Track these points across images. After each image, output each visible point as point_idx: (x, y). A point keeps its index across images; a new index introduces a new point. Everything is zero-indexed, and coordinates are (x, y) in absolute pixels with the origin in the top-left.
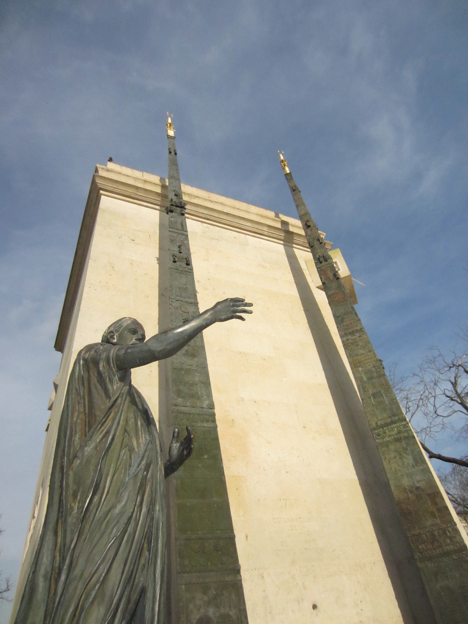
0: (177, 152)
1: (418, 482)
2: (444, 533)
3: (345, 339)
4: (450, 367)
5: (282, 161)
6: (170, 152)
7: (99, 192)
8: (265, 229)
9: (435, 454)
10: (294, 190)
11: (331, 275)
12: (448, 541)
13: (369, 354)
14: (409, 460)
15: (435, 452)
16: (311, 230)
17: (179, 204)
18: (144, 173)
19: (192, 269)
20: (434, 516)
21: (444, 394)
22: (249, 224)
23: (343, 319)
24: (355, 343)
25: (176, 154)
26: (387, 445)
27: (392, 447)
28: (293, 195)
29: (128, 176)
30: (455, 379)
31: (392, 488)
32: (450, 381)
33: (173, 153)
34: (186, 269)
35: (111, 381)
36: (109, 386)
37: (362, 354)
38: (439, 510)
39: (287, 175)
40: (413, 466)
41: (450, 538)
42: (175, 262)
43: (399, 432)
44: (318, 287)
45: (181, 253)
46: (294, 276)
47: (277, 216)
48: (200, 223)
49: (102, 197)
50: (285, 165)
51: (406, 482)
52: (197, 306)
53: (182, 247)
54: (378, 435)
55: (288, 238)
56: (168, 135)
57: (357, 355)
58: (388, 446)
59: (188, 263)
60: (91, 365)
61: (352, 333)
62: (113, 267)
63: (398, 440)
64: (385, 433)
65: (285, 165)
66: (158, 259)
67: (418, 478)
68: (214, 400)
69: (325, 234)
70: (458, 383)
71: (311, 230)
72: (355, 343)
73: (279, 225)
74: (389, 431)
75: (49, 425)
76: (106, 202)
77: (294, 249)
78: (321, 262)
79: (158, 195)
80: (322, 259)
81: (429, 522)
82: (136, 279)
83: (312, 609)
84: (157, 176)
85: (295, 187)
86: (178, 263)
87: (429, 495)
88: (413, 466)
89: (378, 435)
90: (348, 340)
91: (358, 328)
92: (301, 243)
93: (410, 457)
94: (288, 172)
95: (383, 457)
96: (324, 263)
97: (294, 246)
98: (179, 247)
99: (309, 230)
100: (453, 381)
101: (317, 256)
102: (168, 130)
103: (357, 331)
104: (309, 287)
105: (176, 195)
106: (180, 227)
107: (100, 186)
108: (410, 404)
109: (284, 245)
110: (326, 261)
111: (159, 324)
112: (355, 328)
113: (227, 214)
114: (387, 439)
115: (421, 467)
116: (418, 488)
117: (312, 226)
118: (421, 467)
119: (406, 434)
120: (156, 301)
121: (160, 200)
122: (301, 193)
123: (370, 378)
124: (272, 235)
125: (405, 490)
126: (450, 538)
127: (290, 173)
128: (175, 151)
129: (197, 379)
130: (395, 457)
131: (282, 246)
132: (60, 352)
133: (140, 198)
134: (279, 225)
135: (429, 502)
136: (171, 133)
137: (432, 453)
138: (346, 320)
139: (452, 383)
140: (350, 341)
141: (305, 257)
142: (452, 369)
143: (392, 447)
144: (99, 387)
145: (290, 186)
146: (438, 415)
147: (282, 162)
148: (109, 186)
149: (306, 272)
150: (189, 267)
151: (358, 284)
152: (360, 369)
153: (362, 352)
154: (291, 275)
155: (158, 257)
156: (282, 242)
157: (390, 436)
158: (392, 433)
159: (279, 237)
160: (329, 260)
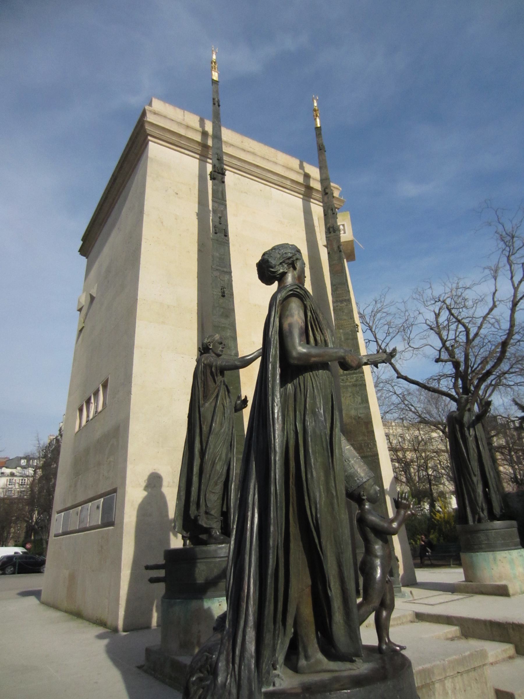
0: (221, 104)
1: (361, 414)
2: (368, 445)
3: (335, 304)
4: (436, 302)
5: (315, 110)
6: (214, 104)
7: (146, 137)
8: (288, 183)
9: (403, 376)
10: (320, 150)
11: (336, 248)
12: (369, 450)
13: (350, 320)
14: (359, 399)
15: (403, 374)
16: (328, 198)
17: (220, 171)
18: (185, 112)
19: (228, 240)
20: (365, 435)
21: (426, 323)
22: (275, 177)
23: (337, 288)
24: (341, 309)
25: (219, 106)
26: (346, 387)
27: (350, 390)
28: (319, 155)
29: (173, 120)
30: (439, 310)
31: (344, 415)
32: (434, 311)
33: (217, 104)
34: (224, 240)
35: (217, 375)
36: (216, 377)
37: (345, 319)
38: (368, 432)
39: (317, 128)
40: (360, 404)
41: (370, 449)
42: (216, 233)
43: (357, 380)
44: (324, 246)
45: (220, 224)
46: (306, 234)
47: (301, 167)
48: (232, 173)
49: (150, 143)
50: (317, 116)
51: (353, 413)
52: (231, 275)
53: (222, 219)
54: (343, 380)
55: (307, 192)
56: (213, 80)
57: (341, 319)
58: (347, 388)
59: (226, 235)
60: (208, 367)
61: (341, 302)
62: (162, 223)
63: (355, 385)
64: (347, 379)
65: (317, 116)
66: (198, 214)
67: (361, 411)
68: (239, 350)
69: (341, 189)
70: (441, 314)
71: (328, 198)
72: (341, 309)
73: (301, 179)
74: (351, 379)
75: (83, 327)
76: (155, 149)
77: (311, 204)
78: (330, 233)
79: (199, 145)
80: (331, 230)
81: (361, 438)
82: (180, 235)
83: (149, 578)
84: (197, 115)
85: (322, 145)
86: (218, 234)
87: (365, 422)
88: (360, 404)
89: (343, 380)
90: (337, 306)
91: (347, 298)
92: (318, 198)
93: (360, 398)
94: (319, 125)
95: (342, 395)
96: (332, 234)
97: (312, 200)
98: (220, 218)
99: (326, 198)
100: (437, 312)
101: (328, 225)
102: (213, 72)
103: (345, 300)
104: (317, 244)
105: (218, 159)
106: (220, 196)
107: (148, 132)
108: (391, 330)
109: (303, 199)
110: (334, 232)
111: (198, 277)
112: (345, 298)
113: (257, 166)
114: (348, 384)
115: (365, 405)
116: (359, 418)
117: (329, 193)
118: (365, 405)
119: (360, 383)
120: (196, 256)
121: (200, 149)
122: (326, 153)
123: (347, 339)
124: (293, 189)
125: (351, 417)
126: (370, 449)
127: (320, 127)
128: (218, 101)
129: (228, 334)
130: (350, 396)
131: (301, 200)
132: (85, 258)
133: (183, 146)
134: (301, 179)
135: (364, 427)
136: (215, 76)
137: (400, 374)
138: (339, 289)
139: (435, 314)
140: (339, 307)
141: (317, 210)
142: (437, 303)
143: (350, 390)
144: (211, 377)
145: (317, 143)
146: (410, 347)
147: (315, 111)
148: (156, 132)
149: (317, 229)
150: (226, 238)
151: (359, 246)
152: (341, 331)
153: (345, 317)
154: (304, 232)
155: (197, 211)
156: (301, 196)
157: (350, 382)
158: (352, 380)
159: (300, 191)
160: (337, 232)
